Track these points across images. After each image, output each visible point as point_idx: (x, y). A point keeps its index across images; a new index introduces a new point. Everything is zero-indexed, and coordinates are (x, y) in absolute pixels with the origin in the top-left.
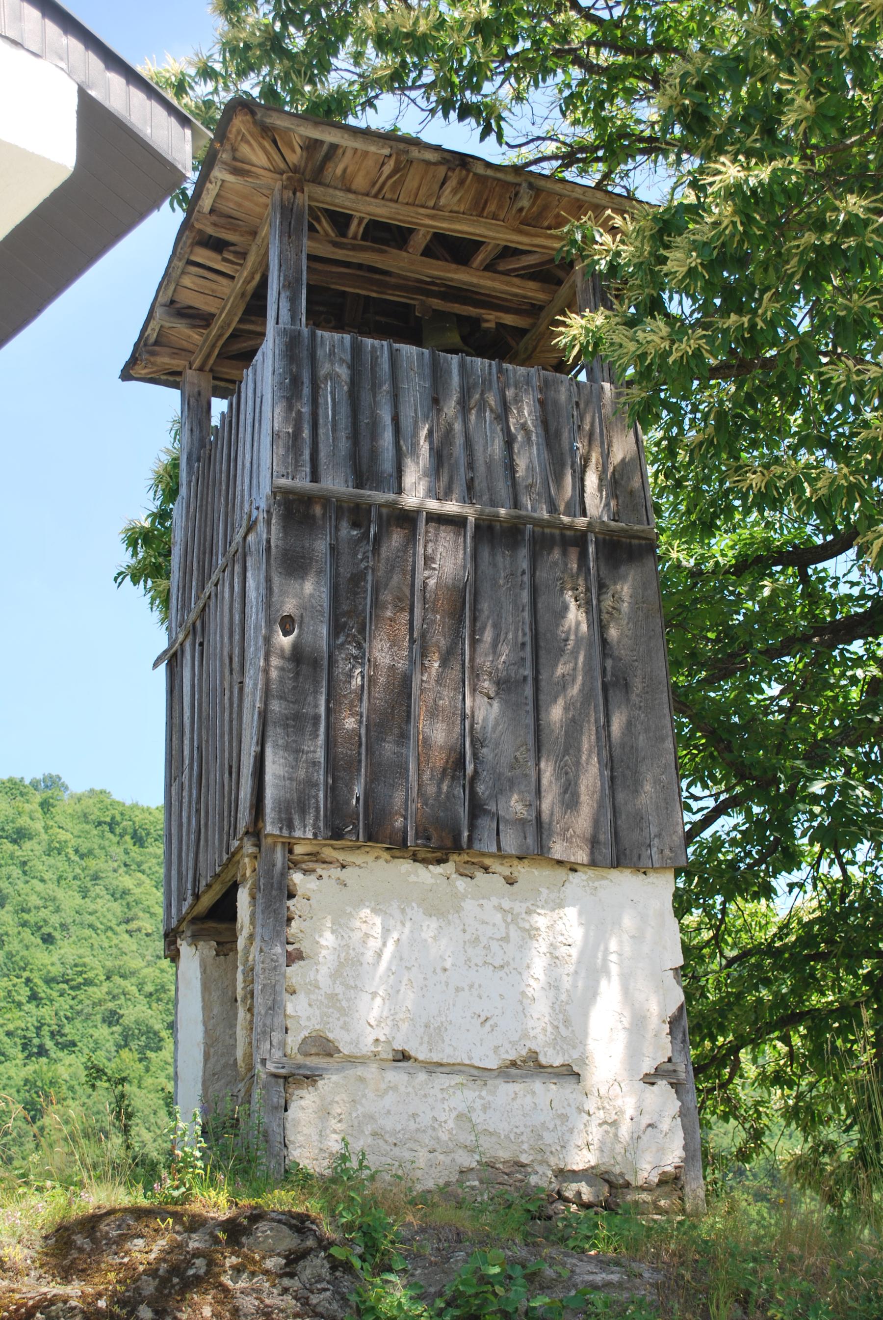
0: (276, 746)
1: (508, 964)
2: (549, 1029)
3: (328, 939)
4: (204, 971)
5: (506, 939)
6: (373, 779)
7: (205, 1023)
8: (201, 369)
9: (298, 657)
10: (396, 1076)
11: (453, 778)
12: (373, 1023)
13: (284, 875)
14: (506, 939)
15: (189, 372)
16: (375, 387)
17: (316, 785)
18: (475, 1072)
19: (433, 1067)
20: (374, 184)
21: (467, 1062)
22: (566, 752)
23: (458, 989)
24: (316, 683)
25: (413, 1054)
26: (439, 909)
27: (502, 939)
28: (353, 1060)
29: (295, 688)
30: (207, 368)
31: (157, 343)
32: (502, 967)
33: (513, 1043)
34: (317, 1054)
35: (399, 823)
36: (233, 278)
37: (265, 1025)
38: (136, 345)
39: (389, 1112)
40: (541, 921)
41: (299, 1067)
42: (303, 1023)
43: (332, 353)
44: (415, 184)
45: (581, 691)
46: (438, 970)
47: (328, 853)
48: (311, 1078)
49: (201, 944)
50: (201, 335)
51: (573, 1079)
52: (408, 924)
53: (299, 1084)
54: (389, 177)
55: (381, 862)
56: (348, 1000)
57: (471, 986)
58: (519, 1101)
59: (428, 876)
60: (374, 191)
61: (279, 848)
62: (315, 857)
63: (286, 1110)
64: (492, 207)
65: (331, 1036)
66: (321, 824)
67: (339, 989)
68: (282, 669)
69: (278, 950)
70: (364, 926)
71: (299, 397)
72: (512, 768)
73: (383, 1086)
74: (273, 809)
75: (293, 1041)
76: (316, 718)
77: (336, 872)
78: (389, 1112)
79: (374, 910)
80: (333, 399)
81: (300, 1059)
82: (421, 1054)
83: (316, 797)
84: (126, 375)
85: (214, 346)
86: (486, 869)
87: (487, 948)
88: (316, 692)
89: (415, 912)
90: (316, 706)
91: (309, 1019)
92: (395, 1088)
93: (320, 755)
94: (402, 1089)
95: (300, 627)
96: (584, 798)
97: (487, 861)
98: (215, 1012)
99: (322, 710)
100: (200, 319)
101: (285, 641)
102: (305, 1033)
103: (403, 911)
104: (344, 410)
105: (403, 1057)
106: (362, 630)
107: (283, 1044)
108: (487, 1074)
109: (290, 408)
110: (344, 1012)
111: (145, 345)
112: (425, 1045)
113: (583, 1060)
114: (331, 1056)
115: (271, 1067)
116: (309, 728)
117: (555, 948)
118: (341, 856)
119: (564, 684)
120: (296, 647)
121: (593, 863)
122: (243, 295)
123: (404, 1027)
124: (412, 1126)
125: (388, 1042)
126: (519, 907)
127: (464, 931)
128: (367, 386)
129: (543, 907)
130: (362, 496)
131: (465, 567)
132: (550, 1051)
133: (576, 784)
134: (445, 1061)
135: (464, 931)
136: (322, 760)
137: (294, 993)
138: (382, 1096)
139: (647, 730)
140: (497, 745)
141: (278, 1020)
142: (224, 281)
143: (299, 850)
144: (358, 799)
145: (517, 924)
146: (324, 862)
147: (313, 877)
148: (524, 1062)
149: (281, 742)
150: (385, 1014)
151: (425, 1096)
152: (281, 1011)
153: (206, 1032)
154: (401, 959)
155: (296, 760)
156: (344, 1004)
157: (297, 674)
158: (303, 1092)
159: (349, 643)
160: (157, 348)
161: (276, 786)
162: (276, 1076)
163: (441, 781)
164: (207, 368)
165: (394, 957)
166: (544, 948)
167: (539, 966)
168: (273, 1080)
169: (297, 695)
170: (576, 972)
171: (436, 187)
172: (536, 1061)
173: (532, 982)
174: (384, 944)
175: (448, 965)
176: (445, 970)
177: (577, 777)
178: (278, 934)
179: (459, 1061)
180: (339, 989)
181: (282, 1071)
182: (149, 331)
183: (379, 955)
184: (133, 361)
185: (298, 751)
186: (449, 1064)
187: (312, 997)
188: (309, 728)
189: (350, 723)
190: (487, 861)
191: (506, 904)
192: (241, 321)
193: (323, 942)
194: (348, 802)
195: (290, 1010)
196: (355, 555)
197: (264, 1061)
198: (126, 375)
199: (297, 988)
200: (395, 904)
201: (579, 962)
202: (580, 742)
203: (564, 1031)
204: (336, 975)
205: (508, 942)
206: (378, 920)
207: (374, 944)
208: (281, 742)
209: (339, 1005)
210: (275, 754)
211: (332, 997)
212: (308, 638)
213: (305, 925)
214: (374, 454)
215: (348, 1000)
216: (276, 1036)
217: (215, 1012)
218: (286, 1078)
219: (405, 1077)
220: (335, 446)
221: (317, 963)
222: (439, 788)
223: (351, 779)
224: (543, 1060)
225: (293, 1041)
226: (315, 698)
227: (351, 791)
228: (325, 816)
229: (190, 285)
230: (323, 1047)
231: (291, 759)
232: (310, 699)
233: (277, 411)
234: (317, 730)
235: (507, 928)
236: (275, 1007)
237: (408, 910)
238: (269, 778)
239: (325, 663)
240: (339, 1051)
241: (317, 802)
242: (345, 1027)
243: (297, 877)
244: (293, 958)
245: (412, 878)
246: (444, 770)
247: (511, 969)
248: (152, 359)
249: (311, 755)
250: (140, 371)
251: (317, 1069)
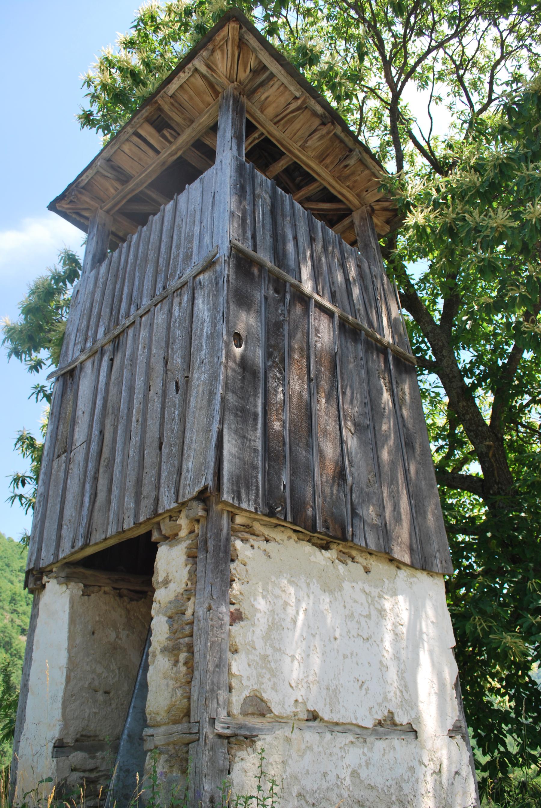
0: (230, 428)
1: (371, 637)
2: (398, 693)
3: (261, 604)
4: (72, 607)
5: (368, 616)
6: (294, 472)
7: (69, 651)
8: (108, 212)
9: (245, 365)
10: (310, 736)
11: (339, 484)
12: (294, 685)
13: (228, 540)
14: (368, 616)
15: (100, 211)
16: (283, 216)
17: (255, 468)
18: (358, 731)
19: (334, 726)
20: (277, 116)
21: (354, 722)
22: (392, 483)
23: (345, 657)
24: (255, 388)
25: (320, 714)
26: (331, 587)
27: (366, 617)
28: (280, 720)
29: (242, 388)
30: (112, 212)
31: (83, 188)
32: (368, 639)
33: (379, 705)
34: (253, 714)
35: (310, 512)
36: (157, 152)
37: (213, 683)
38: (70, 186)
39: (308, 772)
40: (387, 605)
41: (241, 727)
42: (245, 682)
43: (261, 184)
44: (298, 126)
45: (394, 443)
46: (332, 639)
47: (257, 527)
48: (250, 739)
49: (72, 585)
50: (116, 189)
51: (412, 736)
52: (312, 596)
53: (240, 744)
54: (292, 112)
55: (292, 541)
56: (276, 661)
57: (352, 654)
58: (386, 757)
59: (323, 558)
60: (276, 120)
61: (225, 516)
62: (248, 529)
63: (229, 773)
64: (328, 161)
65: (265, 696)
66: (260, 501)
67: (269, 651)
68: (234, 370)
69: (223, 609)
70: (283, 595)
71: (245, 199)
72: (368, 486)
73: (303, 746)
74: (229, 480)
75: (237, 700)
76: (256, 415)
77: (263, 545)
78: (308, 772)
79: (289, 582)
80: (263, 210)
81: (241, 720)
82: (326, 716)
83: (256, 477)
84: (52, 207)
85: (124, 197)
86: (353, 559)
87: (359, 622)
88: (255, 395)
89: (315, 587)
90: (256, 406)
91: (249, 678)
92: (309, 748)
93: (259, 444)
94: (316, 749)
95: (246, 344)
96: (403, 517)
97: (354, 553)
98: (78, 642)
99: (259, 410)
100: (123, 177)
101: (238, 351)
102: (246, 693)
103: (308, 584)
104: (268, 220)
105: (314, 717)
106: (283, 361)
107: (228, 703)
108: (365, 732)
109: (240, 202)
110: (273, 674)
111: (76, 186)
112: (328, 706)
113: (418, 719)
114: (263, 715)
115: (219, 728)
116: (251, 422)
117: (396, 627)
118: (266, 532)
119: (387, 437)
120: (243, 357)
121: (412, 566)
122: (164, 163)
123: (314, 688)
124: (325, 785)
125: (304, 703)
126: (375, 592)
127: (345, 607)
128: (280, 213)
129: (387, 594)
130: (282, 274)
131: (335, 343)
132: (401, 713)
133: (399, 507)
134: (341, 721)
135: (345, 607)
136: (260, 449)
137: (236, 651)
138: (302, 756)
139: (425, 479)
140: (359, 467)
141: (224, 677)
142: (151, 152)
143: (239, 520)
144: (284, 486)
145: (374, 605)
146: (254, 534)
147: (248, 546)
148: (385, 720)
149: (233, 426)
150: (301, 676)
151: (331, 754)
152: (226, 670)
153: (70, 658)
154: (309, 627)
155: (243, 443)
156: (273, 665)
157: (244, 377)
158: (242, 754)
159: (275, 367)
160: (83, 191)
161: (230, 461)
162: (220, 736)
163: (332, 487)
164: (112, 212)
165: (304, 624)
166: (389, 627)
167: (388, 638)
168: (219, 741)
169: (244, 395)
170: (407, 647)
171: (307, 134)
172: (392, 719)
173: (385, 653)
174: (297, 613)
175: (337, 635)
176: (336, 639)
177: (399, 500)
178: (224, 593)
179: (349, 721)
180: (269, 651)
181: (228, 732)
182: (84, 177)
183: (295, 622)
184: (59, 199)
185: (243, 437)
186: (344, 724)
187: (251, 657)
188: (251, 422)
189: (277, 426)
190: (354, 553)
191: (367, 589)
192: (146, 187)
193: (258, 606)
194: (278, 488)
195: (234, 669)
196: (277, 309)
197: (213, 721)
198: (52, 207)
199: (240, 647)
200: (303, 578)
201: (408, 639)
202: (397, 477)
203: (406, 696)
204: (267, 637)
205: (370, 619)
206: (292, 590)
207: (291, 611)
208: (233, 426)
209: (268, 665)
210: (230, 435)
211: (265, 658)
212: (250, 354)
213: (245, 588)
214: (285, 253)
215: (276, 661)
216: (222, 695)
217: (78, 642)
218: (228, 737)
219: (317, 736)
220: (264, 238)
221: (253, 625)
222: (332, 491)
223: (280, 469)
224: (398, 720)
225: (237, 700)
226: (255, 400)
227: (280, 479)
228: (264, 495)
229: (127, 151)
230: (258, 706)
231: (239, 441)
232: (251, 399)
233: (233, 200)
234: (256, 424)
235: (369, 607)
236: (222, 665)
237: (311, 585)
238: (225, 453)
239: (262, 375)
240: (271, 712)
241: (257, 482)
242: (274, 688)
243: (238, 544)
244: (237, 617)
245: (313, 559)
246: (334, 477)
247: (371, 640)
248: (79, 196)
249: (252, 443)
250: (64, 205)
251: (254, 729)
